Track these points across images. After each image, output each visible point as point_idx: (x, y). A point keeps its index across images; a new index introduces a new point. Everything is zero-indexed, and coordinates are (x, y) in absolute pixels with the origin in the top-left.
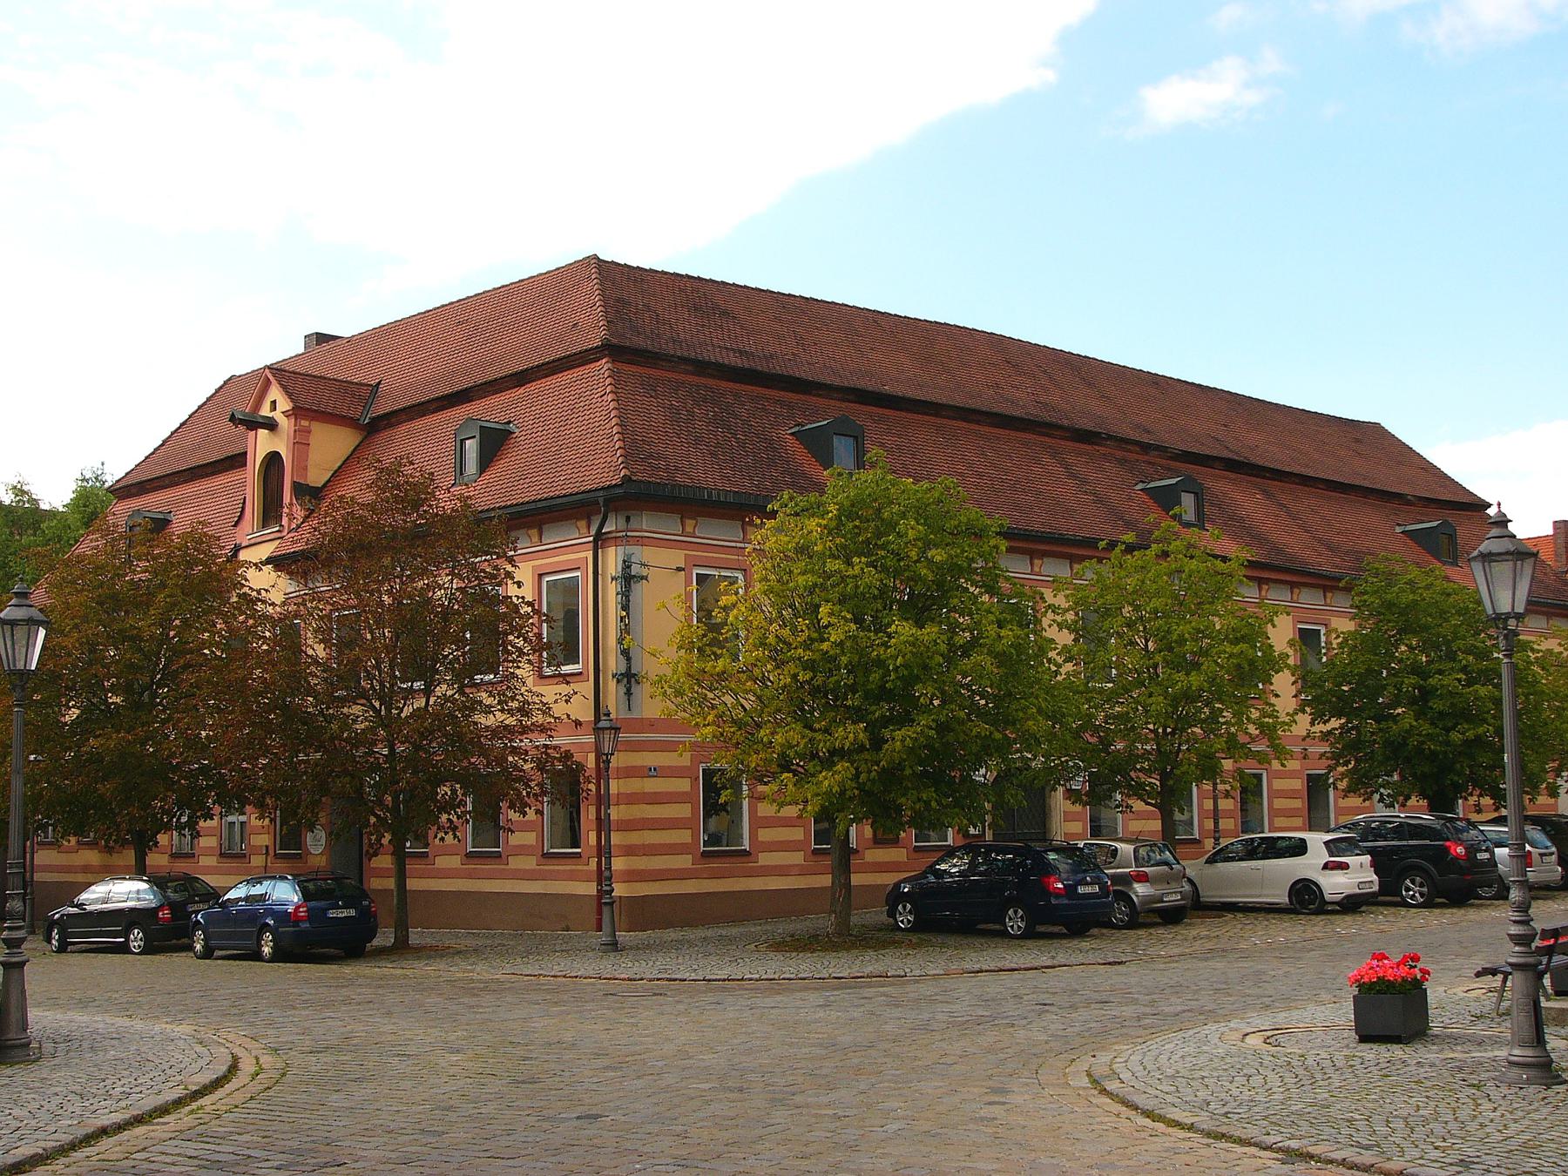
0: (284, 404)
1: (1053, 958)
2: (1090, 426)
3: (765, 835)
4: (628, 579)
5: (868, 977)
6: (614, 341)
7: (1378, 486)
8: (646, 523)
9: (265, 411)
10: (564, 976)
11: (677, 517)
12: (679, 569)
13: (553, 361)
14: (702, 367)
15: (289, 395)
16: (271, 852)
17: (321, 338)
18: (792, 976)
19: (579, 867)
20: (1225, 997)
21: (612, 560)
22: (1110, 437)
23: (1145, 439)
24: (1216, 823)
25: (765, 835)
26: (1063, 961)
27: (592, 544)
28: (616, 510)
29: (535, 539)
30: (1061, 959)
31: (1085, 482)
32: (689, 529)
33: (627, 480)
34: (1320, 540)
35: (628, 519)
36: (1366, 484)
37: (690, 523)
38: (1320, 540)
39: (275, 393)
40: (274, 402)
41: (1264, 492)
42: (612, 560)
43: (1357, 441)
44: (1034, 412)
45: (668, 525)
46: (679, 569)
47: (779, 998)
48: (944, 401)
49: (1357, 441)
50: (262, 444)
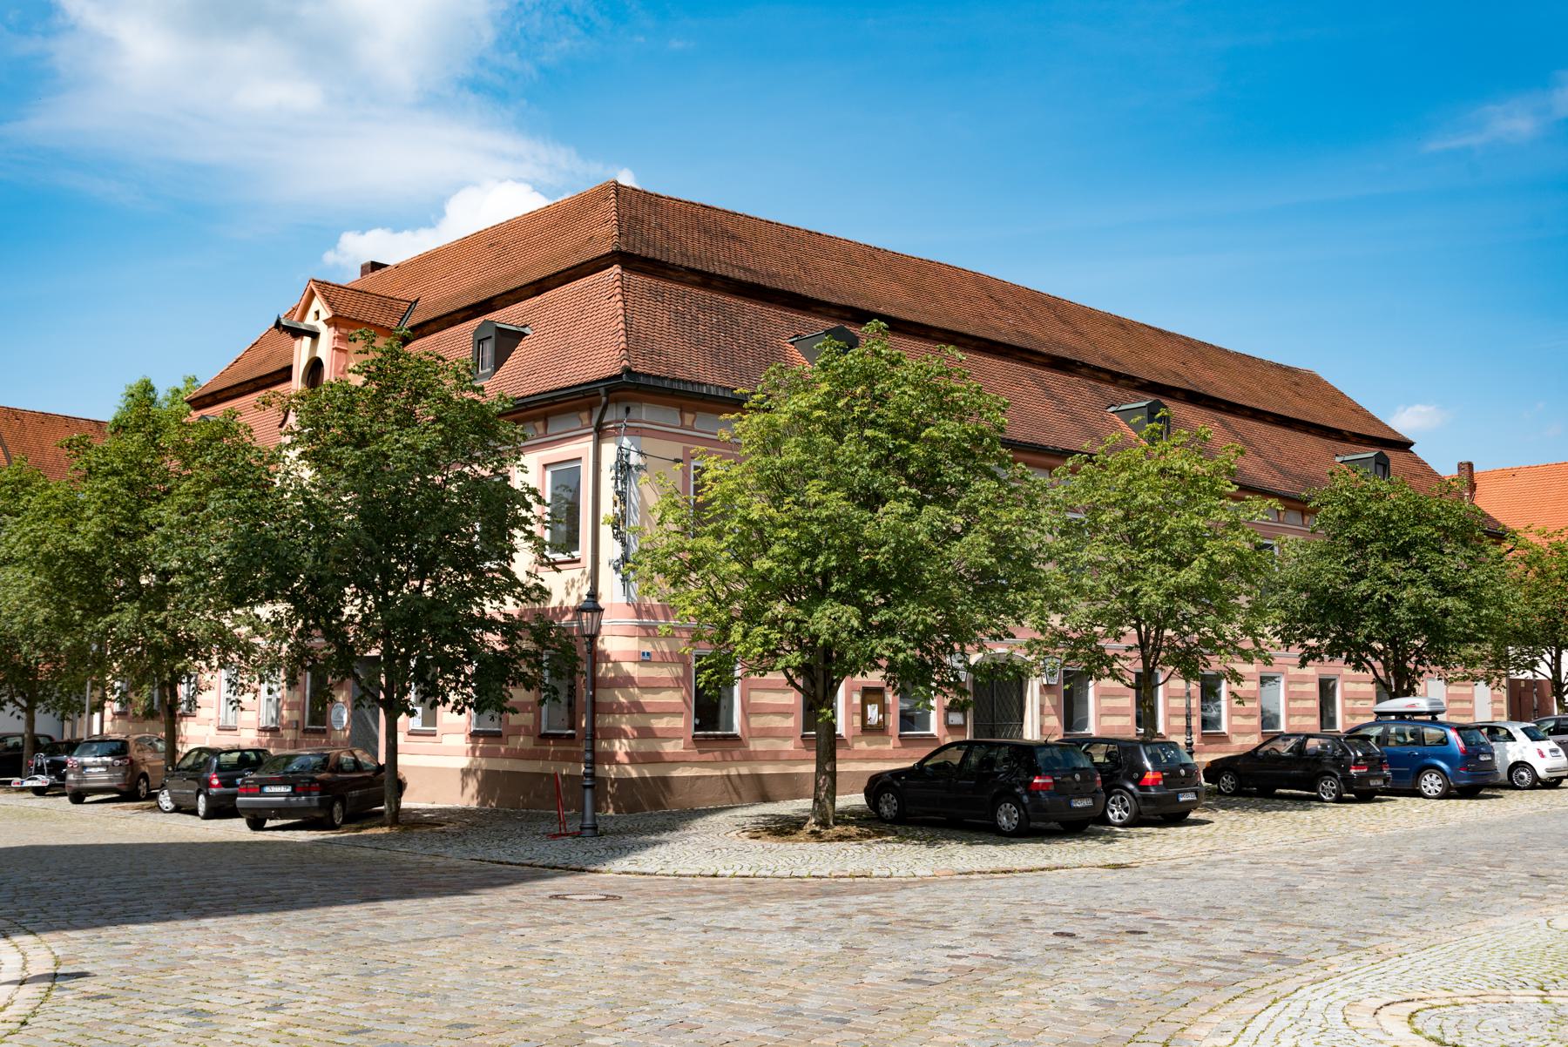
0: (326, 314)
1: (1048, 858)
2: (1066, 354)
3: (756, 722)
4: (624, 469)
5: (850, 876)
6: (624, 248)
7: (1318, 422)
8: (646, 414)
9: (310, 320)
10: (531, 865)
11: (676, 412)
12: (677, 461)
13: (568, 269)
14: (708, 281)
15: (331, 305)
16: (300, 725)
17: (375, 266)
18: (769, 873)
19: (573, 749)
20: (1277, 928)
21: (609, 451)
22: (1084, 365)
23: (1115, 368)
24: (593, 721)
25: (756, 722)
26: (1060, 862)
27: (591, 437)
28: (617, 401)
29: (541, 431)
30: (1056, 860)
31: (1062, 402)
32: (688, 422)
33: (628, 371)
34: (1272, 465)
35: (628, 410)
36: (1308, 419)
37: (689, 418)
38: (1272, 465)
39: (318, 304)
40: (317, 313)
41: (1222, 422)
42: (609, 451)
43: (1297, 384)
44: (1016, 341)
45: (665, 417)
46: (677, 461)
47: (743, 912)
48: (934, 324)
49: (1297, 384)
50: (301, 353)
